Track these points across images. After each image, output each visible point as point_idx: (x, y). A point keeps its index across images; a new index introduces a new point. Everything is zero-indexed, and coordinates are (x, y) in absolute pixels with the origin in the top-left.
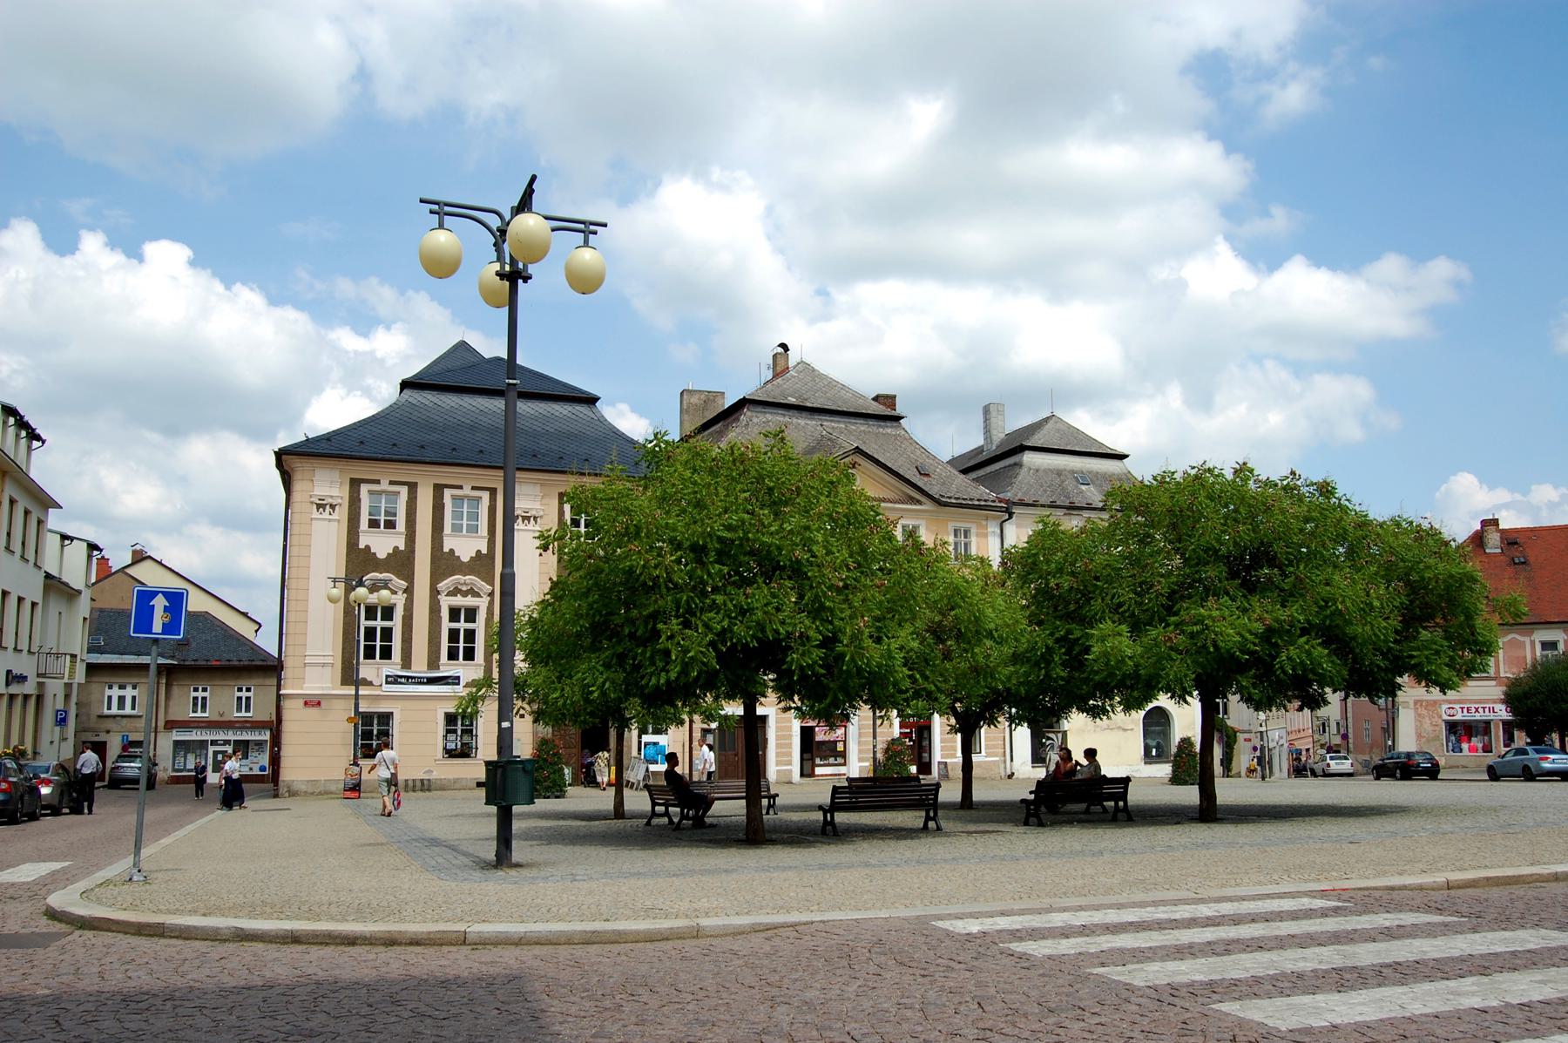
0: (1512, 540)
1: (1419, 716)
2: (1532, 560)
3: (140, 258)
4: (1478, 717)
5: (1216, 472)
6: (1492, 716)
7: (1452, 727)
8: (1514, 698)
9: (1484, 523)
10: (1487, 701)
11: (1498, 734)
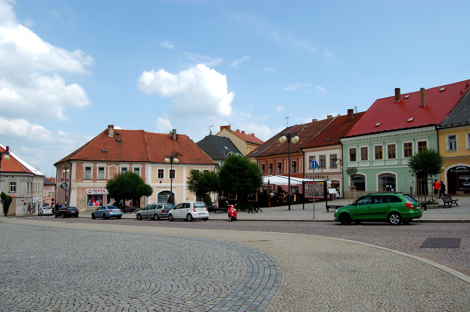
0: (117, 133)
2: (122, 140)
3: (228, 93)
4: (99, 193)
6: (103, 193)
7: (90, 196)
8: (110, 187)
10: (100, 188)
11: (105, 199)
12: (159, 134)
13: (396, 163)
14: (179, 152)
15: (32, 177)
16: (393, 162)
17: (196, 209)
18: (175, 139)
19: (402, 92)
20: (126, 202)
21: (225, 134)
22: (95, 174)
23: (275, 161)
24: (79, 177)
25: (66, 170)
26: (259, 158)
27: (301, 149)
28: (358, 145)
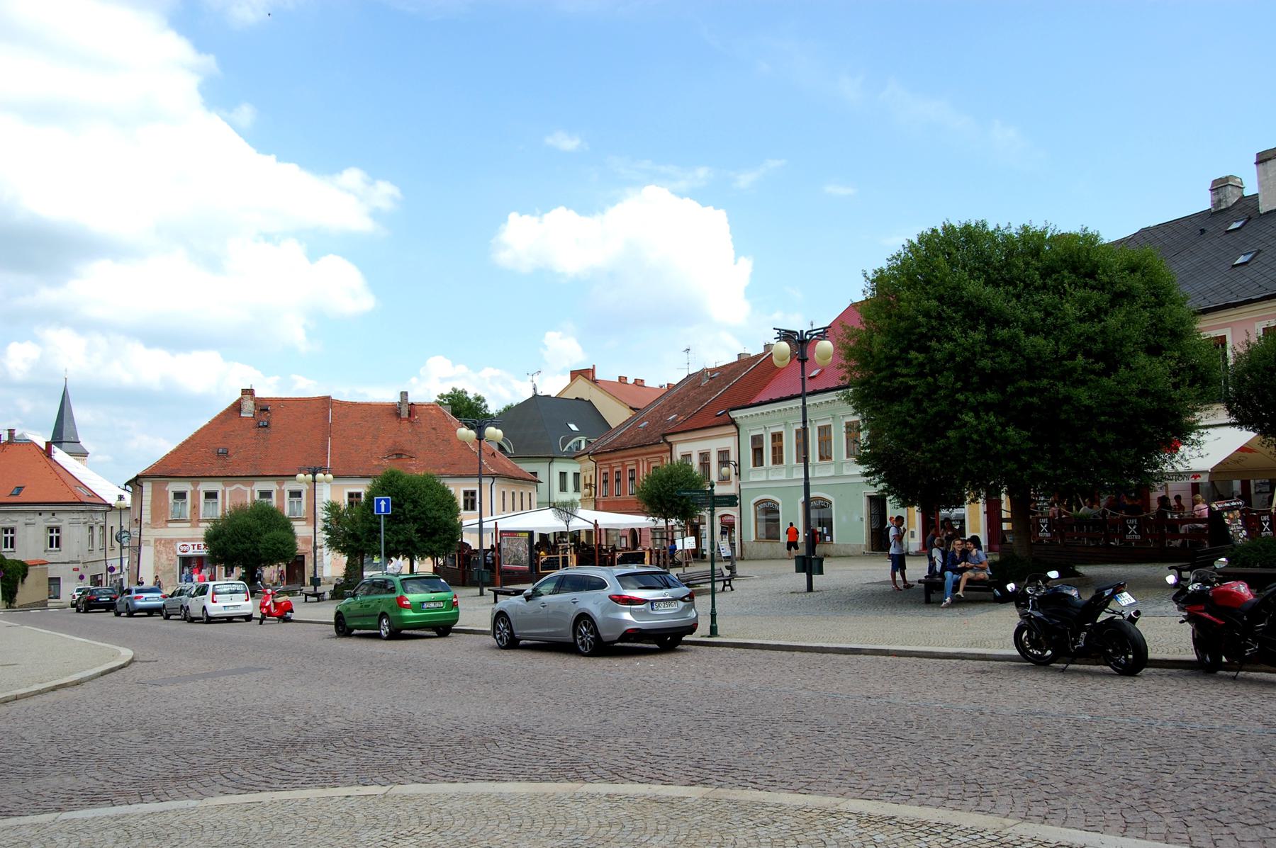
0: (263, 407)
1: (158, 552)
5: (1201, 370)
9: (245, 392)
12: (369, 405)
13: (832, 473)
14: (407, 447)
15: (106, 512)
16: (779, 474)
17: (217, 597)
18: (405, 414)
19: (17, 434)
20: (416, 564)
21: (583, 390)
22: (195, 507)
23: (611, 468)
24: (160, 517)
25: (314, 474)
26: (600, 457)
27: (664, 435)
28: (786, 424)
